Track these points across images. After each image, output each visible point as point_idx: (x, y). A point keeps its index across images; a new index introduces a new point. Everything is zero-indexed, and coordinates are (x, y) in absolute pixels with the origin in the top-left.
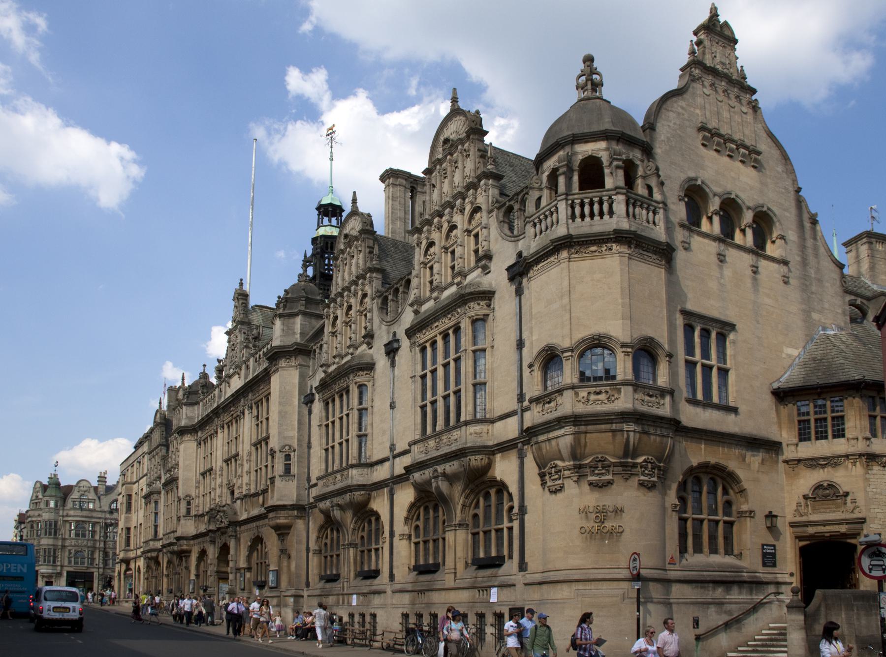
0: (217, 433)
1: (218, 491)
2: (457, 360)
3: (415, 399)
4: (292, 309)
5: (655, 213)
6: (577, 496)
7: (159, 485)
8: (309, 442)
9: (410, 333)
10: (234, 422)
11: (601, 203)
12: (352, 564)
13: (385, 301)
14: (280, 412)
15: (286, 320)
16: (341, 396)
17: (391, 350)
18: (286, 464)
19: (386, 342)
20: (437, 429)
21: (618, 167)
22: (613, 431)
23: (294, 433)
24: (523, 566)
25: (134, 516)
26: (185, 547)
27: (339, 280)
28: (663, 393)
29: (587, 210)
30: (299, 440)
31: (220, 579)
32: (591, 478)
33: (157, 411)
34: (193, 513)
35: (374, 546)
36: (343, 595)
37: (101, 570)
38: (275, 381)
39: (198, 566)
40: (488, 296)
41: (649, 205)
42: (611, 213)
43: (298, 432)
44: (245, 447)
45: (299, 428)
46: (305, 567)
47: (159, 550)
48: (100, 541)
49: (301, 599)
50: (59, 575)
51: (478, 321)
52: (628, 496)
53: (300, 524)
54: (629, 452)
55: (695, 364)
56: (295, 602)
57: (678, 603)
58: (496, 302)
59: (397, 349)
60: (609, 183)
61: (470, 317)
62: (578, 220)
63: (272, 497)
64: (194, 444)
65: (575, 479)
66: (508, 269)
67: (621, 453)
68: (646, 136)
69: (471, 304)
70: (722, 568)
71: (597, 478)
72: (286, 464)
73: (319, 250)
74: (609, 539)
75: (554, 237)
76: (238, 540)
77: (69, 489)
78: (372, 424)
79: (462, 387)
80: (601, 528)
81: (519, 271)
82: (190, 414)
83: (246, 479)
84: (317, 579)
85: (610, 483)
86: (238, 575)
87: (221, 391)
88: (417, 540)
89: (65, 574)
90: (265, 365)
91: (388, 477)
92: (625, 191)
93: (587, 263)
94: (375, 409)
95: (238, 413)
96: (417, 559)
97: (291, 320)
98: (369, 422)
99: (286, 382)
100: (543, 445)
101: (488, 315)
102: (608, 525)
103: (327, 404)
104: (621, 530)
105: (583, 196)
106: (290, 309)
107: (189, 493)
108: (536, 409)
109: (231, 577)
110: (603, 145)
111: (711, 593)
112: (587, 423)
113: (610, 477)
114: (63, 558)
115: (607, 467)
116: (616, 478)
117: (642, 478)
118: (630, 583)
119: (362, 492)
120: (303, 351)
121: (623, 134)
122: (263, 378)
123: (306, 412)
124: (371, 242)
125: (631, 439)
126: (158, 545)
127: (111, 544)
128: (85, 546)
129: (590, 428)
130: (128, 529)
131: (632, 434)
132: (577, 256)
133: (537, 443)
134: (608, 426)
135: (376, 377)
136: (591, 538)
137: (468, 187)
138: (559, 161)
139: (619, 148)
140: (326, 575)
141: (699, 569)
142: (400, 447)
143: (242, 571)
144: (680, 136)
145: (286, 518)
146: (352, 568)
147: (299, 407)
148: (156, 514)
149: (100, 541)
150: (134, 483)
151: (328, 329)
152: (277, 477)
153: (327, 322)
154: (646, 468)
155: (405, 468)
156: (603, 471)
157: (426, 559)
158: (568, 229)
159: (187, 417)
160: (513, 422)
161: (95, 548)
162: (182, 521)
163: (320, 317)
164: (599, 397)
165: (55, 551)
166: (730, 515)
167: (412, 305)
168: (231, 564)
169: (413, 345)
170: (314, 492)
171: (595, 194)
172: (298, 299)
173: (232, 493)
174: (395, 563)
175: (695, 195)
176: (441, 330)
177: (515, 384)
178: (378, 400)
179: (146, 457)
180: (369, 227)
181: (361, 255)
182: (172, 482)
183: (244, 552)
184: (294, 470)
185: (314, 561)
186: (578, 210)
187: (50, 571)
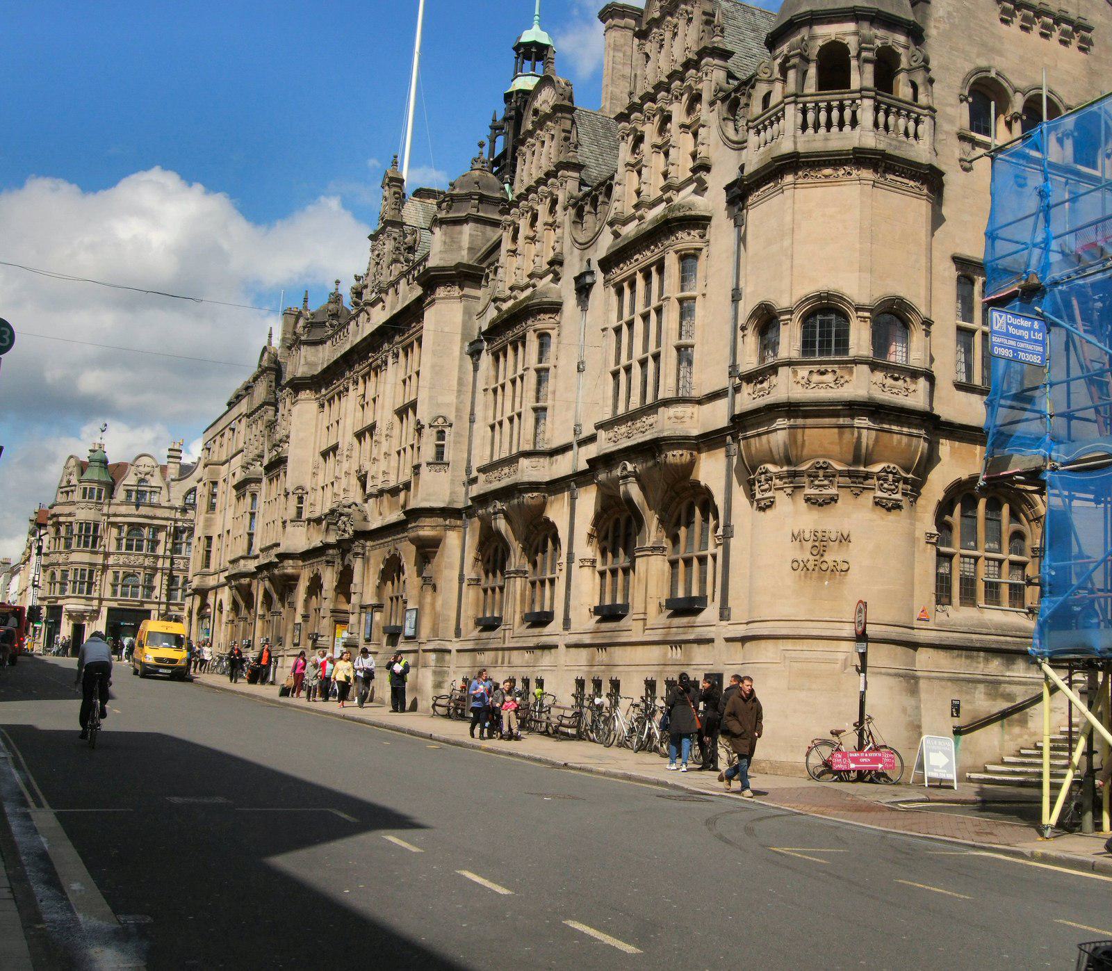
0: (347, 390)
1: (344, 482)
2: (659, 311)
3: (606, 363)
4: (459, 211)
5: (917, 122)
6: (791, 514)
7: (258, 469)
8: (472, 414)
9: (607, 264)
10: (372, 374)
11: (841, 109)
12: (518, 602)
13: (580, 214)
14: (433, 366)
15: (451, 228)
16: (647, 277)
17: (583, 289)
18: (437, 446)
19: (577, 274)
20: (647, 403)
21: (866, 61)
22: (840, 427)
23: (451, 398)
24: (724, 614)
25: (218, 516)
26: (290, 571)
27: (525, 174)
28: (914, 374)
29: (823, 116)
30: (458, 410)
31: (337, 622)
32: (808, 491)
33: (265, 349)
34: (305, 515)
35: (549, 575)
36: (503, 649)
37: (163, 607)
38: (431, 316)
39: (307, 601)
40: (700, 222)
41: (909, 112)
42: (854, 123)
43: (458, 397)
44: (384, 416)
45: (459, 391)
46: (455, 605)
47: (252, 575)
48: (164, 557)
49: (447, 657)
50: (95, 614)
51: (688, 258)
52: (856, 516)
53: (452, 539)
54: (860, 457)
55: (972, 332)
56: (437, 660)
57: (929, 678)
58: (712, 232)
59: (591, 285)
60: (855, 82)
61: (676, 252)
62: (810, 131)
63: (415, 496)
64: (314, 406)
65: (789, 491)
66: (728, 188)
67: (850, 457)
68: (915, 13)
69: (680, 234)
70: (1003, 631)
71: (817, 492)
72: (437, 446)
73: (513, 113)
74: (830, 579)
75: (776, 153)
76: (366, 560)
77: (121, 468)
78: (554, 393)
79: (662, 349)
80: (820, 560)
81: (740, 194)
82: (311, 359)
83: (382, 465)
84: (471, 624)
85: (833, 499)
86: (363, 615)
87: (358, 326)
88: (603, 568)
89: (104, 612)
90: (418, 291)
91: (570, 472)
92: (872, 94)
93: (818, 193)
94: (560, 371)
95: (379, 362)
96: (602, 598)
97: (458, 228)
98: (550, 388)
99: (448, 319)
100: (752, 440)
101: (701, 249)
102: (829, 557)
103: (620, 292)
104: (845, 567)
105: (819, 98)
106: (455, 212)
107: (301, 483)
108: (747, 389)
109: (353, 619)
110: (850, 27)
111: (981, 665)
112: (806, 415)
113: (833, 491)
114: (104, 586)
115: (830, 476)
116: (842, 493)
117: (879, 494)
118: (853, 643)
119: (535, 494)
120: (468, 276)
121: (879, 12)
122: (411, 315)
123: (471, 367)
124: (569, 123)
125: (864, 441)
126: (251, 566)
127: (180, 564)
128: (140, 566)
129: (810, 421)
130: (209, 538)
131: (864, 432)
132: (806, 180)
133: (745, 438)
134: (833, 421)
135: (562, 323)
136: (806, 576)
137: (688, 65)
138: (791, 48)
139: (867, 30)
140: (485, 618)
141: (965, 629)
142: (588, 430)
143: (369, 610)
144: (969, 9)
145: (433, 527)
146: (518, 609)
147: (461, 359)
148: (253, 515)
149: (164, 557)
150: (223, 464)
151: (506, 245)
152: (424, 465)
153: (505, 234)
154: (886, 480)
155: (589, 461)
156: (826, 482)
157: (614, 598)
158: (795, 143)
159: (307, 363)
160: (722, 406)
161: (155, 570)
162: (289, 527)
163: (495, 224)
164: (824, 378)
165: (91, 572)
166: (1020, 552)
167: (611, 224)
168: (354, 599)
169: (606, 282)
170: (475, 490)
171: (834, 97)
172: (469, 197)
173: (364, 486)
174: (572, 603)
175: (985, 95)
176: (642, 265)
177: (727, 351)
178: (562, 358)
179: (244, 420)
180: (566, 103)
181: (554, 144)
182: (277, 465)
183: (373, 579)
184: (448, 455)
185: (470, 595)
186: (811, 116)
187: (82, 607)
